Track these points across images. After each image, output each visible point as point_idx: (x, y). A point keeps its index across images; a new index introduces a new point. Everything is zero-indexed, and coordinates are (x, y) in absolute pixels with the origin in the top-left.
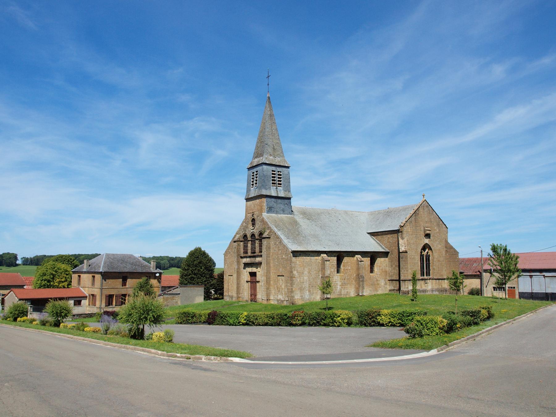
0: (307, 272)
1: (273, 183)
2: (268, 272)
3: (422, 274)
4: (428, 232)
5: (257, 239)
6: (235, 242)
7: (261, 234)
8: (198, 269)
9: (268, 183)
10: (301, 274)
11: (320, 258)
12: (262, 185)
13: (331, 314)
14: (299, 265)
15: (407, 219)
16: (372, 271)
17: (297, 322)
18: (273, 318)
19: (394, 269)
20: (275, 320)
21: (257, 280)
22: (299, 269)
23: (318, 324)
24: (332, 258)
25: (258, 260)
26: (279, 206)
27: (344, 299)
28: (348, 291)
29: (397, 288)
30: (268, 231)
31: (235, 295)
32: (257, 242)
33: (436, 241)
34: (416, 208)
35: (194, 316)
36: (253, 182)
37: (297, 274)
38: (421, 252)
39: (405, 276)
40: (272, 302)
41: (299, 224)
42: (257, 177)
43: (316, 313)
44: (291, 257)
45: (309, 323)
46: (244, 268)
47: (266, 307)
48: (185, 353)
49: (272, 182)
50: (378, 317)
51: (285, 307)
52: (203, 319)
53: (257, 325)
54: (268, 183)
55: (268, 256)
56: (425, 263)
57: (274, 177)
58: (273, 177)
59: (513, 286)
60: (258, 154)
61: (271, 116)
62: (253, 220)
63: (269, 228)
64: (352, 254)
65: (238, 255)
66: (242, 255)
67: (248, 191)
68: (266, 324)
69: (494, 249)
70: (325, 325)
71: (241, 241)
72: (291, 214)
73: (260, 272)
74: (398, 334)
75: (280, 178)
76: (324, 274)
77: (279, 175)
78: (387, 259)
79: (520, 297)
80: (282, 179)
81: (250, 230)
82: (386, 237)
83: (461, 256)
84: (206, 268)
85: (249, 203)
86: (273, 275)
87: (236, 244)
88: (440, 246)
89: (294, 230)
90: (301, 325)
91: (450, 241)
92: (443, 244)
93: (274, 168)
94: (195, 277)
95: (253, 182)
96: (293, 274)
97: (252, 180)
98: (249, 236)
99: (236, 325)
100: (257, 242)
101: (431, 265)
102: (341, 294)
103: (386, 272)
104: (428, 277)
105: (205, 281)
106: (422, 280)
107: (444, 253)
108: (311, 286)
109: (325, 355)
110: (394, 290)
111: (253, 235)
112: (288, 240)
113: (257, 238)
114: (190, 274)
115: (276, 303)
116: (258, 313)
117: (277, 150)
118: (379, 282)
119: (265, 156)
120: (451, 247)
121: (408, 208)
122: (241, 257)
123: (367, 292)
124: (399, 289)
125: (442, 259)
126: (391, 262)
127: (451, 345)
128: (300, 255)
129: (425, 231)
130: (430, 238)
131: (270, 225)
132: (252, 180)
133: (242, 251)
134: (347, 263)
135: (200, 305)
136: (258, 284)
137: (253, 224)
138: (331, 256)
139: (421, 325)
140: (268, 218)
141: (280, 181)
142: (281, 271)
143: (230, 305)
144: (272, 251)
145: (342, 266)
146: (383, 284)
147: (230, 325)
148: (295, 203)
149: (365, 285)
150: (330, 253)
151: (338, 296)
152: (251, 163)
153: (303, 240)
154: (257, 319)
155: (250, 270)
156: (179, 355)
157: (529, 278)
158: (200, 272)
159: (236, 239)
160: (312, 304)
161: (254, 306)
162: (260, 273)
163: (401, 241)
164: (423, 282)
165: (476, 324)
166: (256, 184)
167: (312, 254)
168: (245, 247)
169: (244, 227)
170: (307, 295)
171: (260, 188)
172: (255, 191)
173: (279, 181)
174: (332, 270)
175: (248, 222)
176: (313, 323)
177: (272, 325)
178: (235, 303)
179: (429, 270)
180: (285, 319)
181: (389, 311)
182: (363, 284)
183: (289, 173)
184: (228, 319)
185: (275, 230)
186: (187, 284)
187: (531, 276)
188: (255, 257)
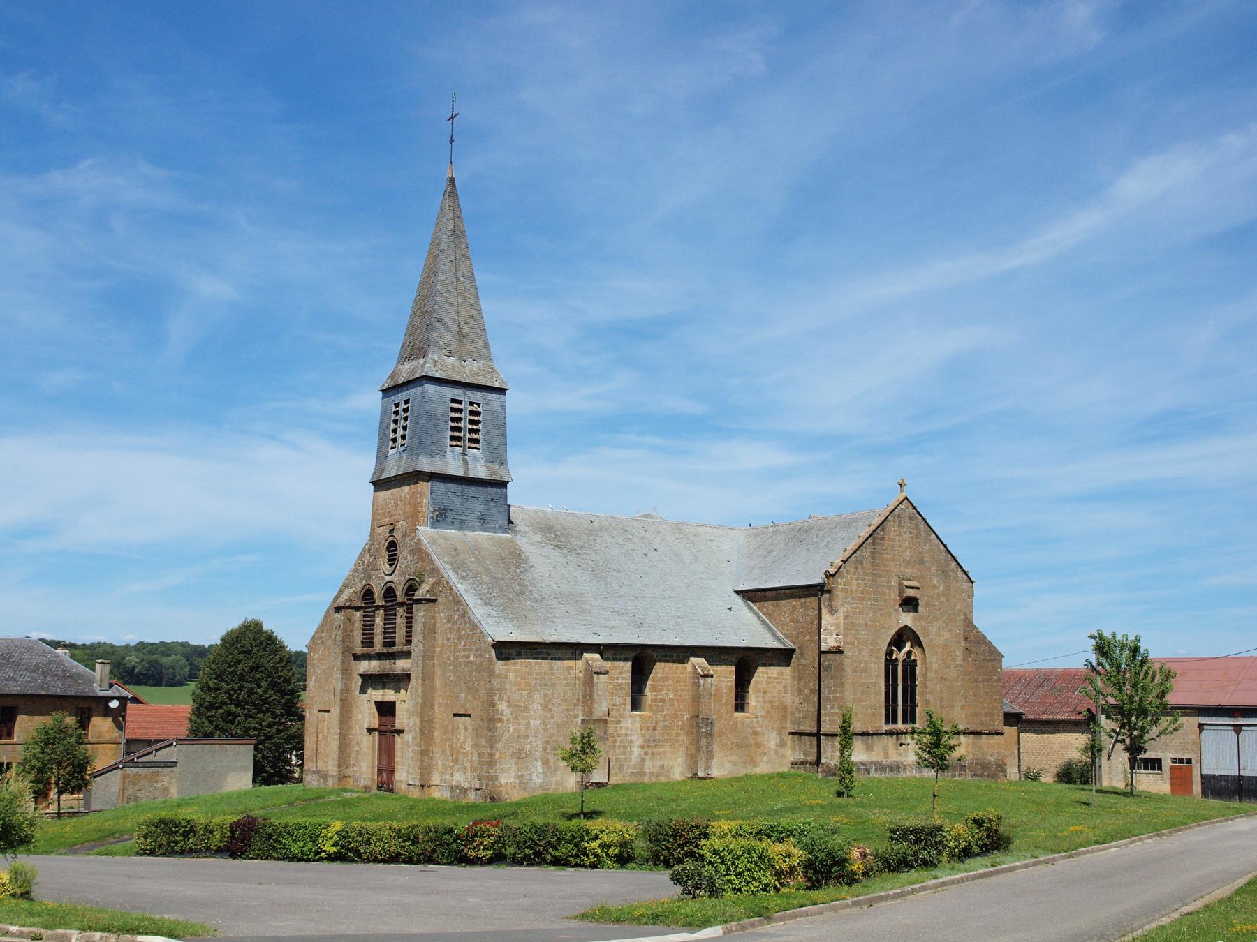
0: (537, 706)
1: (452, 438)
2: (426, 705)
3: (891, 717)
6: (338, 610)
7: (411, 588)
8: (249, 690)
9: (441, 436)
10: (521, 710)
11: (579, 664)
12: (421, 443)
13: (575, 829)
14: (517, 684)
15: (848, 553)
16: (740, 705)
17: (481, 853)
18: (415, 841)
19: (807, 700)
20: (419, 849)
21: (398, 726)
22: (515, 697)
23: (536, 859)
24: (616, 664)
25: (401, 665)
26: (469, 504)
29: (812, 758)
30: (431, 581)
31: (332, 769)
32: (400, 611)
33: (936, 619)
34: (876, 521)
35: (191, 831)
36: (395, 431)
37: (507, 711)
38: (890, 653)
40: (436, 794)
41: (526, 561)
42: (406, 419)
46: (363, 691)
47: (412, 807)
48: (34, 925)
49: (450, 433)
50: (702, 842)
51: (470, 808)
52: (216, 839)
53: (368, 861)
54: (441, 436)
55: (428, 656)
56: (901, 686)
57: (459, 420)
58: (453, 419)
59: (1186, 757)
60: (413, 350)
61: (457, 234)
62: (392, 546)
63: (435, 571)
64: (679, 653)
65: (347, 650)
66: (358, 651)
67: (382, 458)
68: (394, 859)
69: (1103, 647)
70: (557, 862)
71: (357, 609)
72: (506, 531)
73: (405, 702)
74: (655, 885)
75: (478, 423)
76: (591, 713)
77: (471, 413)
78: (787, 670)
79: (1205, 793)
80: (480, 426)
82: (787, 606)
83: (1008, 664)
84: (272, 685)
85: (381, 494)
86: (441, 715)
88: (947, 635)
90: (490, 861)
92: (958, 629)
93: (457, 393)
94: (238, 711)
95: (395, 431)
97: (393, 426)
98: (378, 593)
99: (308, 860)
100: (400, 611)
101: (918, 690)
102: (642, 774)
103: (784, 708)
104: (909, 726)
105: (270, 726)
106: (890, 733)
107: (959, 654)
110: (804, 763)
111: (389, 592)
112: (488, 608)
113: (400, 599)
114: (224, 703)
116: (371, 825)
117: (471, 337)
118: (760, 739)
119: (433, 355)
120: (982, 640)
121: (857, 520)
122: (357, 658)
123: (721, 767)
124: (818, 762)
125: (951, 673)
126: (800, 679)
127: (782, 919)
128: (519, 655)
129: (901, 588)
130: (916, 610)
132: (393, 426)
133: (358, 637)
134: (664, 679)
135: (242, 795)
136: (398, 739)
137: (392, 560)
139: (722, 862)
140: (434, 541)
141: (477, 431)
142: (464, 701)
143: (316, 798)
144: (440, 640)
145: (647, 691)
147: (292, 860)
149: (716, 747)
150: (610, 651)
151: (634, 779)
152: (392, 376)
154: (368, 842)
155: (378, 695)
156: (14, 929)
157: (1231, 733)
160: (549, 801)
161: (386, 804)
162: (405, 706)
163: (826, 619)
164: (891, 741)
165: (927, 864)
166: (403, 437)
167: (553, 652)
168: (368, 626)
169: (365, 567)
170: (536, 775)
172: (401, 458)
173: (471, 431)
174: (618, 701)
175: (378, 550)
176: (526, 857)
177: (410, 861)
178: (330, 793)
179: (914, 706)
180: (444, 846)
182: (709, 745)
183: (503, 407)
184: (286, 840)
185: (453, 577)
186: (211, 734)
187: (1238, 729)
188: (392, 656)
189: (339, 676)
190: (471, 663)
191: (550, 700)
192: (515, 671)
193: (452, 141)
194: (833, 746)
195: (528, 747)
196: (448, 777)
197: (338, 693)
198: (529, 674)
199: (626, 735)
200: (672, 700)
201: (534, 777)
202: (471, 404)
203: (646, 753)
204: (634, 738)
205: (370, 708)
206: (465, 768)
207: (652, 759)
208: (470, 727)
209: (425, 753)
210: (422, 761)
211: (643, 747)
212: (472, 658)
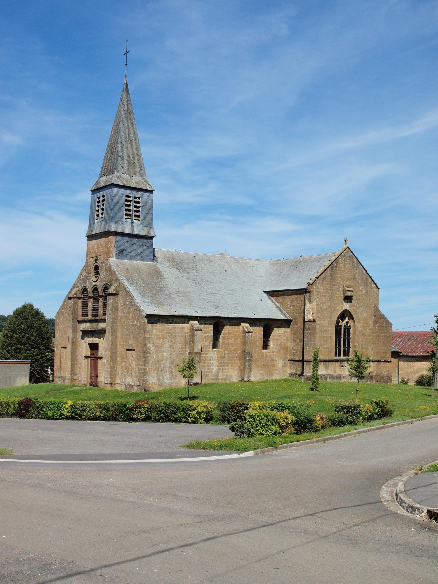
0: (167, 345)
1: (126, 215)
3: (337, 353)
4: (349, 293)
5: (101, 296)
6: (70, 298)
7: (106, 289)
9: (121, 213)
10: (159, 348)
11: (188, 326)
12: (110, 217)
13: (185, 405)
14: (157, 335)
16: (265, 346)
17: (140, 416)
18: (108, 410)
19: (297, 344)
20: (110, 414)
21: (100, 355)
22: (157, 342)
23: (166, 419)
24: (206, 326)
25: (101, 326)
26: (134, 248)
27: (218, 385)
28: (229, 374)
29: (299, 372)
30: (116, 285)
33: (360, 306)
34: (333, 258)
36: (98, 211)
37: (152, 348)
38: (338, 322)
40: (118, 388)
41: (162, 275)
42: (103, 205)
43: (164, 403)
44: (144, 323)
45: (155, 417)
46: (83, 338)
49: (125, 212)
50: (245, 412)
51: (135, 394)
52: (12, 409)
53: (85, 419)
54: (121, 213)
55: (114, 321)
57: (129, 206)
58: (127, 205)
60: (107, 171)
61: (129, 113)
62: (97, 268)
63: (117, 280)
64: (236, 321)
65: (74, 318)
66: (80, 319)
67: (91, 224)
68: (98, 418)
70: (176, 421)
71: (80, 298)
72: (153, 261)
73: (103, 344)
74: (222, 432)
76: (193, 349)
77: (136, 202)
78: (288, 330)
80: (140, 209)
82: (289, 299)
83: (395, 328)
84: (39, 335)
85: (91, 242)
86: (120, 350)
87: (71, 302)
88: (366, 314)
89: (154, 284)
90: (144, 420)
92: (371, 311)
93: (129, 192)
94: (22, 347)
95: (98, 211)
97: (97, 208)
98: (90, 290)
99: (56, 419)
100: (101, 299)
101: (351, 340)
102: (217, 379)
103: (286, 348)
104: (346, 358)
106: (337, 361)
107: (371, 324)
109: (110, 454)
110: (295, 374)
111: (95, 290)
112: (144, 298)
115: (123, 388)
116: (87, 403)
117: (136, 164)
118: (275, 363)
119: (117, 173)
122: (79, 322)
123: (256, 376)
125: (367, 332)
126: (294, 334)
127: (282, 448)
129: (344, 291)
130: (351, 302)
131: (120, 277)
132: (97, 208)
133: (80, 312)
134: (229, 333)
136: (100, 361)
138: (205, 324)
139: (255, 421)
141: (138, 212)
142: (132, 343)
143: (61, 389)
145: (221, 339)
146: (280, 365)
147: (48, 419)
148: (157, 243)
149: (253, 366)
152: (97, 183)
153: (166, 300)
154: (85, 411)
158: (29, 341)
159: (71, 295)
160: (172, 391)
161: (94, 392)
162: (103, 345)
164: (337, 365)
165: (352, 423)
166: (102, 214)
167: (178, 321)
168: (85, 307)
169: (83, 278)
170: (167, 379)
171: (107, 221)
173: (136, 211)
174: (206, 344)
175: (89, 270)
177: (105, 419)
178: (67, 387)
180: (121, 412)
181: (261, 403)
182: (250, 365)
183: (151, 200)
184: (46, 409)
185: (126, 283)
186: (8, 359)
188: (97, 321)
190: (135, 325)
193: (126, 65)
195: (163, 365)
196: (124, 380)
197: (70, 339)
199: (210, 360)
200: (232, 344)
202: (136, 198)
203: (220, 369)
204: (214, 362)
205: (86, 347)
206: (132, 375)
207: (222, 372)
208: (134, 356)
210: (111, 372)
211: (218, 366)
212: (135, 322)
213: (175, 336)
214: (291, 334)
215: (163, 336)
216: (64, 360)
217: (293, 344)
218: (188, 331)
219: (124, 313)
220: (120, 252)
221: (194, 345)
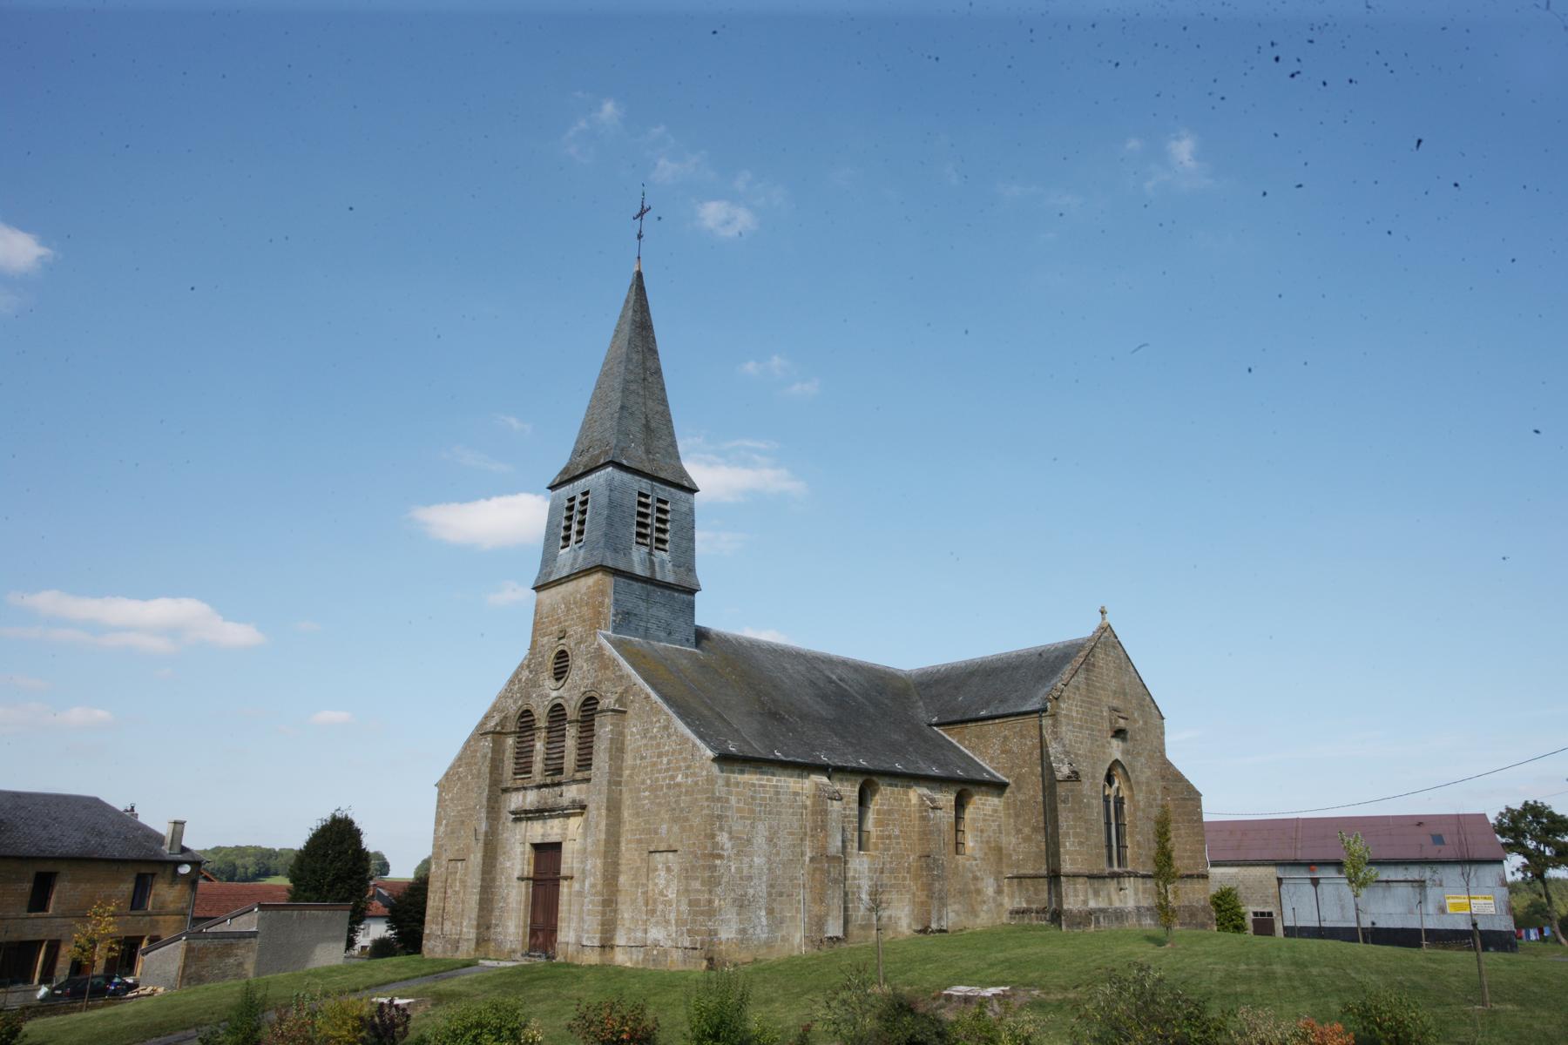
4: (1122, 723)
10: (743, 845)
14: (739, 810)
19: (1027, 839)
25: (571, 793)
26: (654, 611)
31: (469, 932)
37: (728, 845)
39: (1074, 862)
40: (621, 958)
55: (615, 781)
59: (1266, 910)
81: (551, 691)
91: (1170, 756)
93: (645, 485)
96: (715, 845)
108: (776, 892)
118: (980, 885)
120: (1179, 778)
126: (1017, 816)
132: (564, 523)
137: (560, 673)
146: (990, 891)
155: (539, 831)
169: (522, 682)
189: (483, 815)
190: (679, 785)
191: (776, 833)
192: (738, 794)
193: (640, 237)
194: (1075, 890)
196: (639, 934)
197: (481, 837)
198: (753, 798)
200: (897, 837)
201: (758, 930)
202: (659, 500)
205: (523, 853)
206: (668, 922)
208: (676, 868)
209: (609, 902)
210: (604, 914)
212: (679, 779)
213: (779, 813)
214: (1009, 816)
215: (752, 811)
216: (456, 893)
217: (1014, 840)
218: (808, 803)
219: (642, 758)
220: (623, 619)
221: (826, 836)
